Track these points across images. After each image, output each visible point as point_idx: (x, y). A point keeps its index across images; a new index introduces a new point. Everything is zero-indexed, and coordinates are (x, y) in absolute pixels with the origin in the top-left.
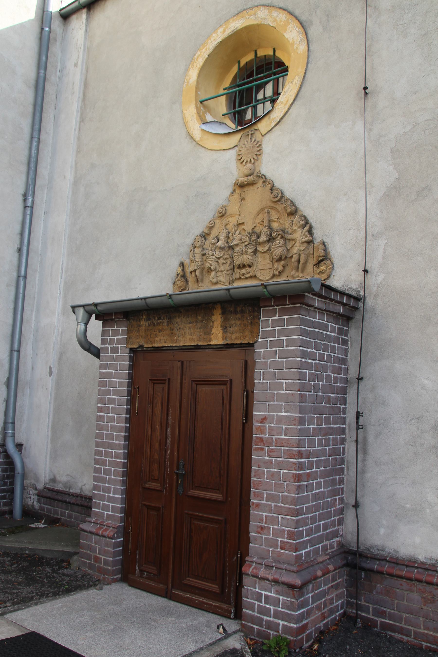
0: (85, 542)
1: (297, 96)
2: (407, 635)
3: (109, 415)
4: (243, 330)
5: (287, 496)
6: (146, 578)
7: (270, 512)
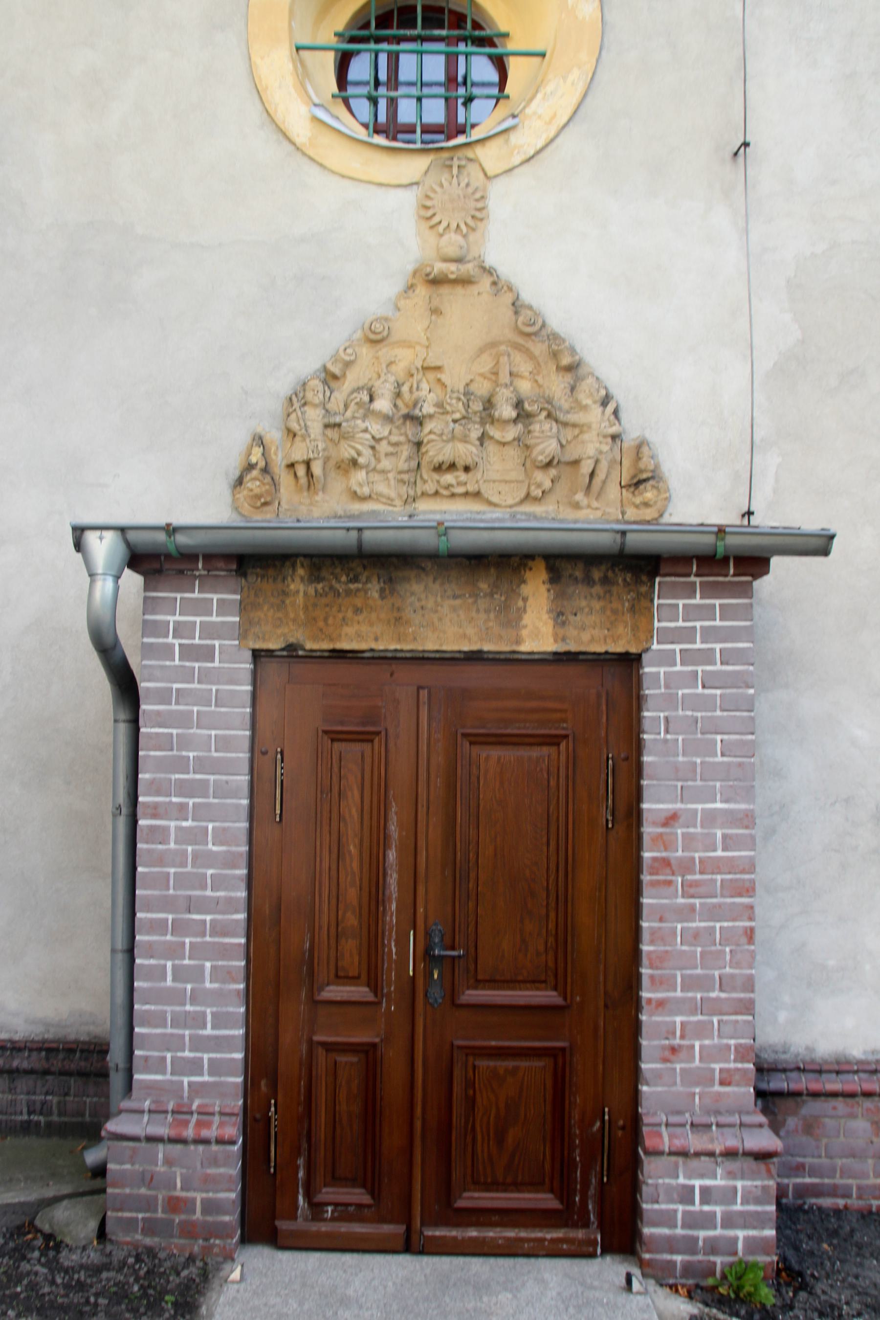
0: (128, 1166)
1: (575, 112)
2: (844, 1196)
3: (185, 824)
4: (612, 623)
5: (732, 976)
6: (333, 1219)
7: (693, 1012)
